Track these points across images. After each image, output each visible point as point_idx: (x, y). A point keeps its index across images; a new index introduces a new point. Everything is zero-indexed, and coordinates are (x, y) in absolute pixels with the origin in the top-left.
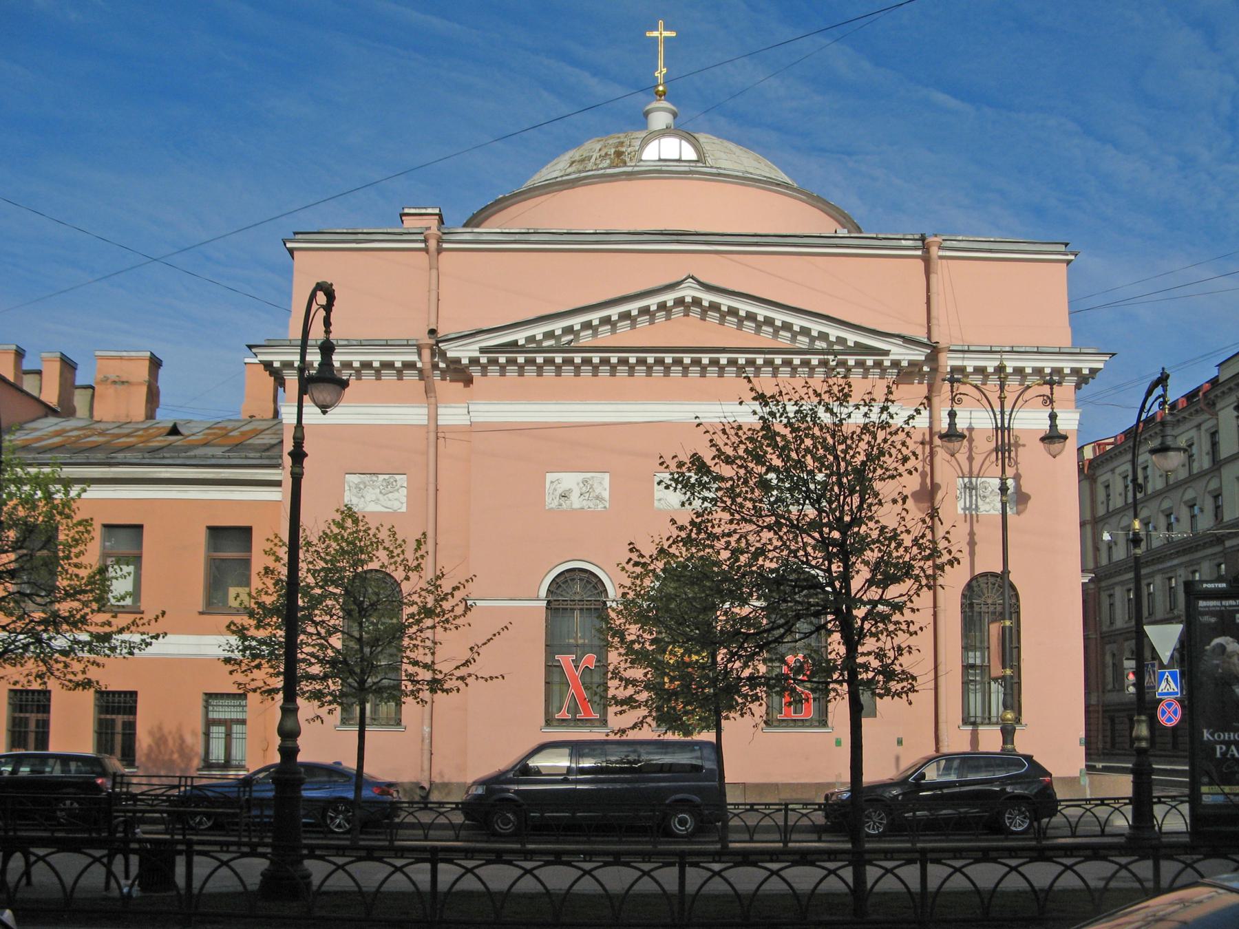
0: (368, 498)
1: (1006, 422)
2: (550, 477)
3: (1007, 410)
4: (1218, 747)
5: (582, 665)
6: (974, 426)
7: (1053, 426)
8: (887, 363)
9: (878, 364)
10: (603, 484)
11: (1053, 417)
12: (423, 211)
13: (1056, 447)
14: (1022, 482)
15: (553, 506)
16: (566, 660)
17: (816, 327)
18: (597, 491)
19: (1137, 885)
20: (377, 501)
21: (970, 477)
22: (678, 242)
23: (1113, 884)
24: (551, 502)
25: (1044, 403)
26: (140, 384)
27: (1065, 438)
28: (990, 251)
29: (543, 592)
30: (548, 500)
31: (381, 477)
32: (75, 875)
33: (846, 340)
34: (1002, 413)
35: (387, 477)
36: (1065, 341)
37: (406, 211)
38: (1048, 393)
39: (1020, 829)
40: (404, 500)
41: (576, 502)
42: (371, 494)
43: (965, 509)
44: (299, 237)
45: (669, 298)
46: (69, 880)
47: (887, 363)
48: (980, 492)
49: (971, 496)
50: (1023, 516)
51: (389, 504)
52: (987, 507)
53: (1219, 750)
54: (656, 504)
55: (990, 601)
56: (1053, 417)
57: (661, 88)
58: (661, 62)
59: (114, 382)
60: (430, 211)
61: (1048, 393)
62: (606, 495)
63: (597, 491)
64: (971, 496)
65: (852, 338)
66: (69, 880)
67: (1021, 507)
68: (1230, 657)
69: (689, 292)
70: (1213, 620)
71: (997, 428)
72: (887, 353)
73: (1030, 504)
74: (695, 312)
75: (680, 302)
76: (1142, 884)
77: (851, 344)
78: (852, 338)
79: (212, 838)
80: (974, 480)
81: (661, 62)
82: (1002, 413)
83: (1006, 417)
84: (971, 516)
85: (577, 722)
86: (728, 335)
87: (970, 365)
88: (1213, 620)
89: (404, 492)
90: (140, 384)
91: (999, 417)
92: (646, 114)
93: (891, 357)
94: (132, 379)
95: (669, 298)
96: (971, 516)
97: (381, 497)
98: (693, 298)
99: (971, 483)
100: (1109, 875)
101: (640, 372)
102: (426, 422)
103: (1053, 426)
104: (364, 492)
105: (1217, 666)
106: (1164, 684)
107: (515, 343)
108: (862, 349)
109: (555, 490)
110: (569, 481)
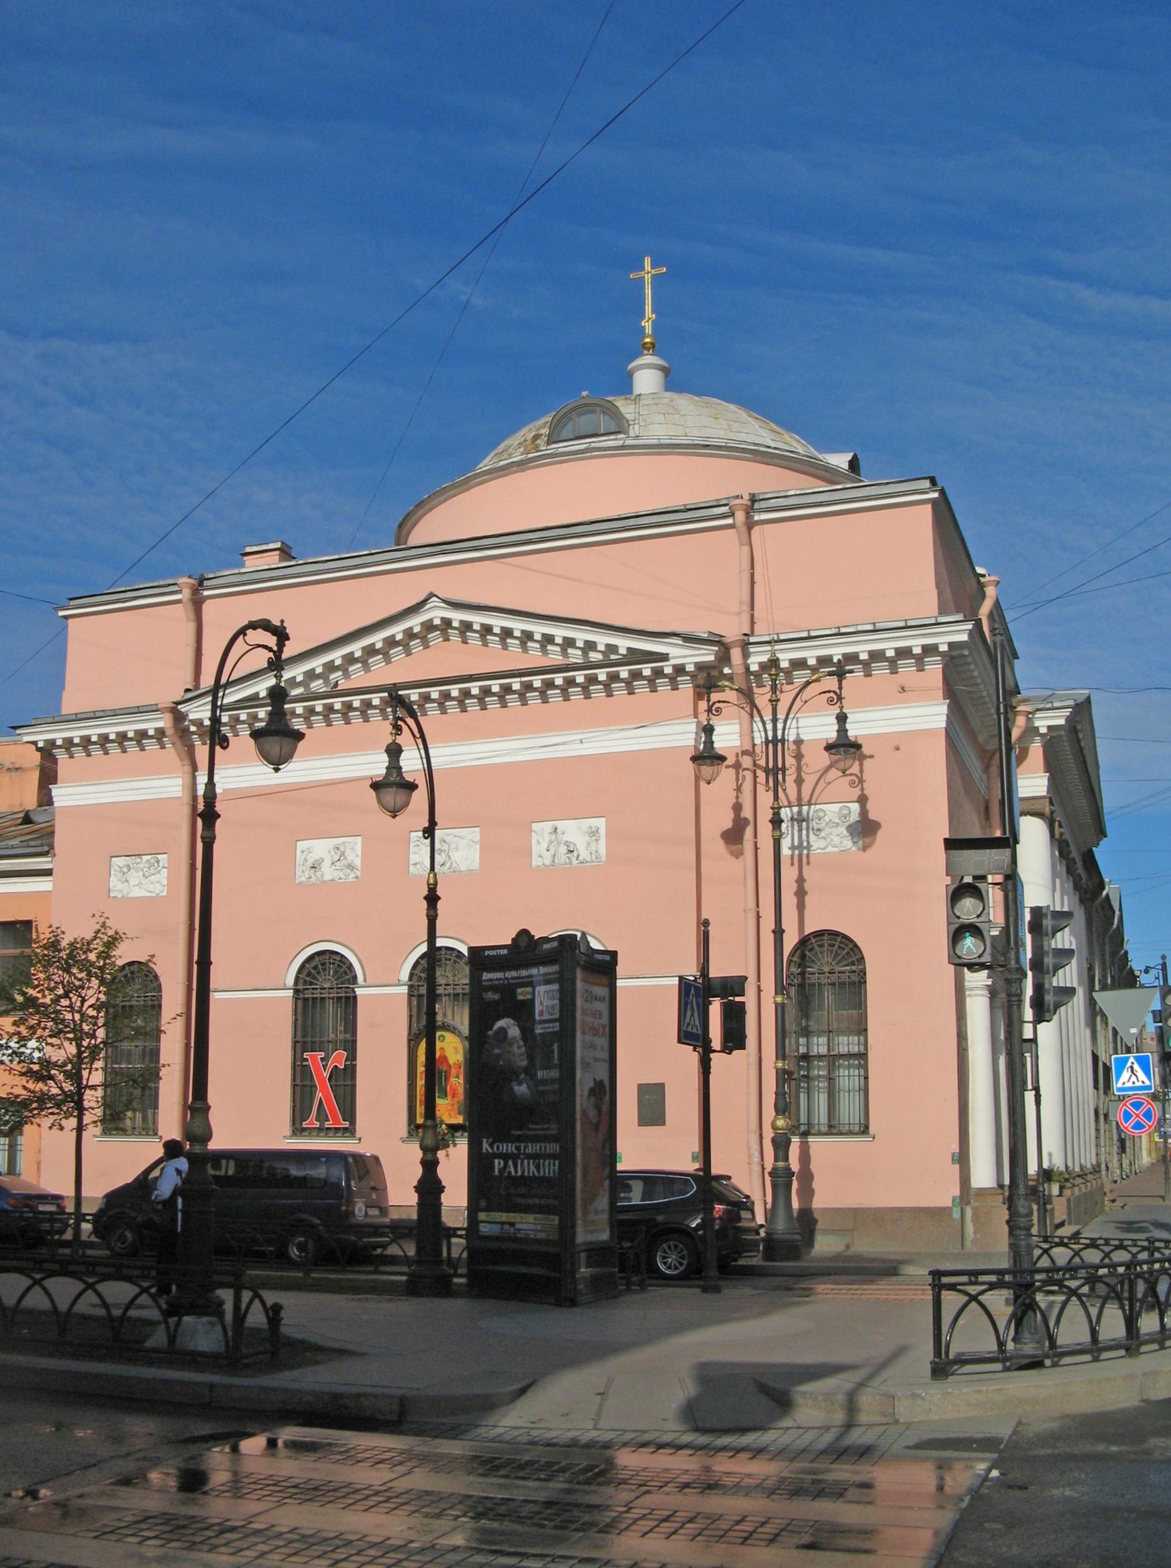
0: (132, 883)
1: (779, 733)
2: (301, 845)
3: (781, 716)
4: (496, 1161)
5: (331, 1065)
6: (802, 737)
7: (842, 731)
8: (668, 670)
9: (658, 673)
10: (354, 848)
11: (842, 719)
12: (265, 547)
13: (707, 770)
14: (869, 806)
15: (303, 879)
16: (314, 1058)
17: (581, 636)
18: (349, 859)
19: (102, 1312)
20: (140, 885)
21: (800, 805)
22: (443, 553)
23: (132, 1313)
24: (302, 875)
25: (830, 701)
26: (31, 769)
27: (722, 759)
28: (821, 504)
29: (290, 981)
30: (299, 872)
31: (145, 858)
32: (69, 1301)
33: (616, 647)
34: (775, 720)
35: (148, 857)
36: (934, 610)
37: (248, 550)
38: (835, 688)
39: (662, 1267)
40: (165, 882)
41: (328, 872)
42: (134, 877)
43: (793, 848)
44: (73, 603)
45: (415, 623)
46: (63, 1307)
47: (668, 670)
48: (813, 824)
49: (800, 830)
50: (869, 852)
51: (151, 888)
52: (822, 844)
53: (498, 1164)
54: (412, 868)
55: (826, 969)
56: (842, 719)
57: (648, 340)
58: (648, 308)
59: (9, 769)
60: (271, 546)
61: (835, 688)
62: (358, 862)
63: (349, 859)
64: (800, 830)
65: (624, 644)
66: (63, 1307)
67: (867, 840)
68: (511, 1045)
69: (436, 613)
70: (497, 997)
71: (767, 742)
72: (664, 657)
73: (880, 833)
74: (435, 637)
75: (429, 626)
76: (108, 1311)
77: (623, 651)
78: (624, 644)
79: (393, 1278)
80: (805, 808)
81: (648, 308)
82: (775, 720)
83: (780, 726)
84: (800, 856)
85: (323, 1131)
86: (494, 658)
87: (811, 657)
88: (497, 997)
89: (165, 872)
90: (31, 769)
91: (769, 727)
92: (630, 375)
93: (672, 662)
94: (25, 765)
95: (415, 623)
96: (800, 856)
97: (143, 880)
98: (443, 619)
99: (800, 813)
100: (127, 1301)
101: (374, 715)
102: (180, 794)
103: (842, 731)
104: (128, 876)
105: (499, 1056)
106: (1126, 1075)
107: (255, 697)
108: (636, 656)
109: (306, 860)
110: (320, 848)
